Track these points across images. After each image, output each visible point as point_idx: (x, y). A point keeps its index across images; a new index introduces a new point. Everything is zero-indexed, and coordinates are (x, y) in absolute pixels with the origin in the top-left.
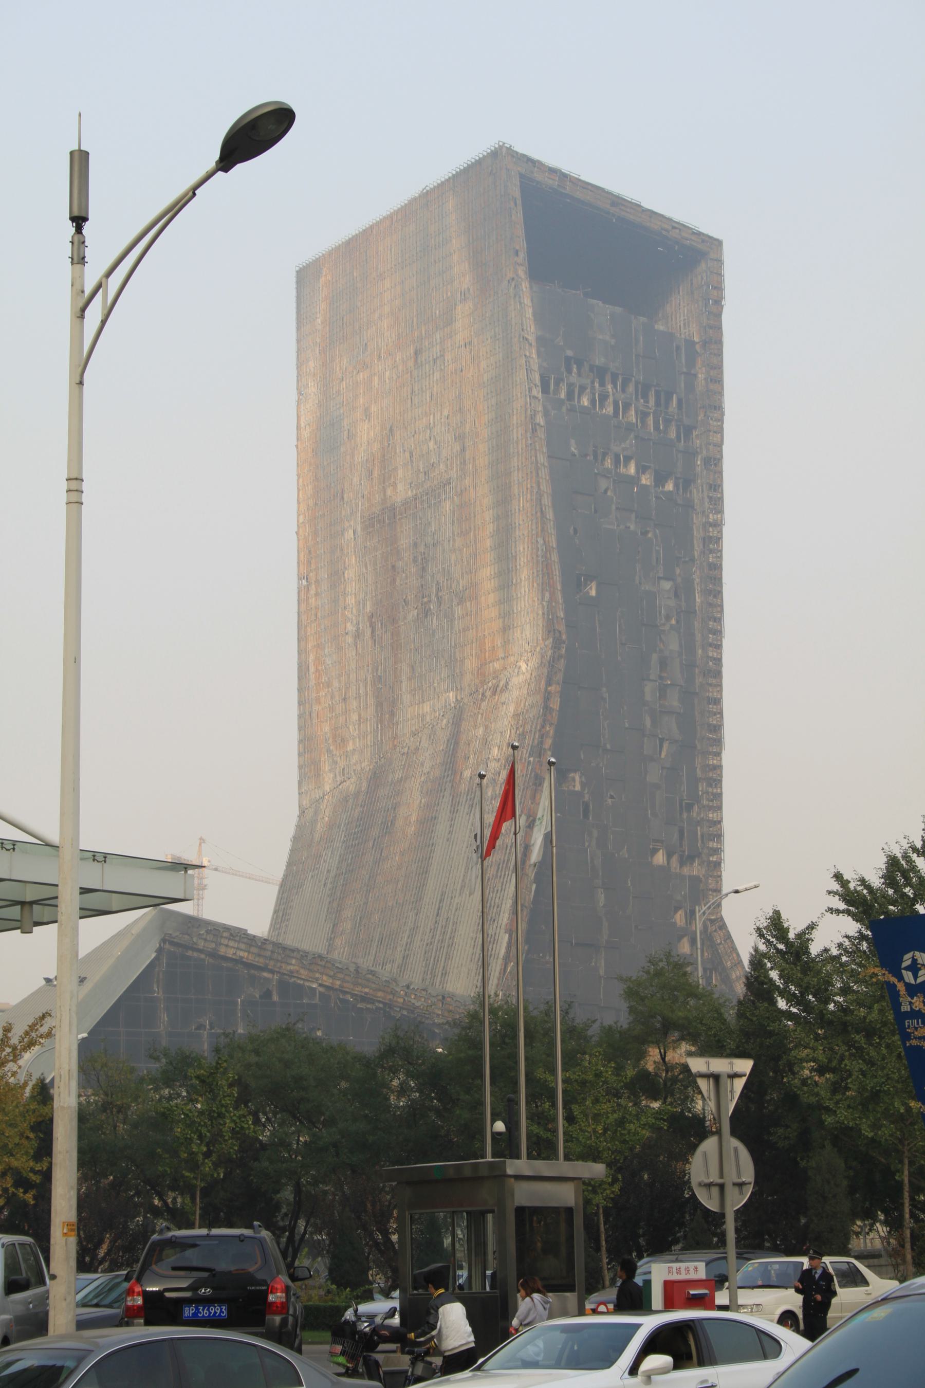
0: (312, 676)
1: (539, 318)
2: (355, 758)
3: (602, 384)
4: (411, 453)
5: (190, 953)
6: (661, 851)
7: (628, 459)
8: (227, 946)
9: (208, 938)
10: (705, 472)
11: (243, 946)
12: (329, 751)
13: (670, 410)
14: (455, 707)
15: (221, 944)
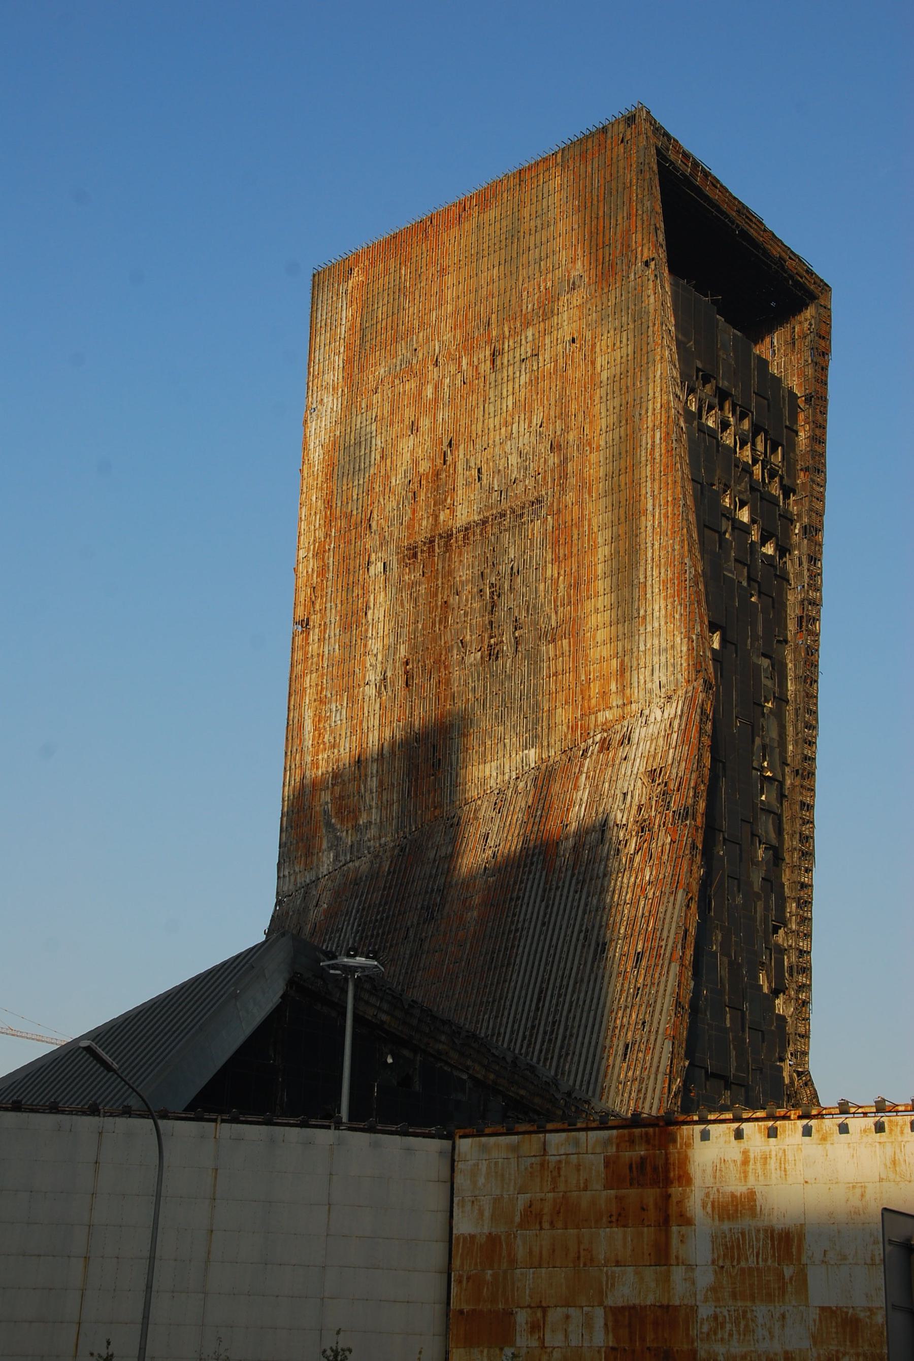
2: (373, 832)
4: (479, 471)
7: (743, 504)
11: (385, 1006)
12: (329, 825)
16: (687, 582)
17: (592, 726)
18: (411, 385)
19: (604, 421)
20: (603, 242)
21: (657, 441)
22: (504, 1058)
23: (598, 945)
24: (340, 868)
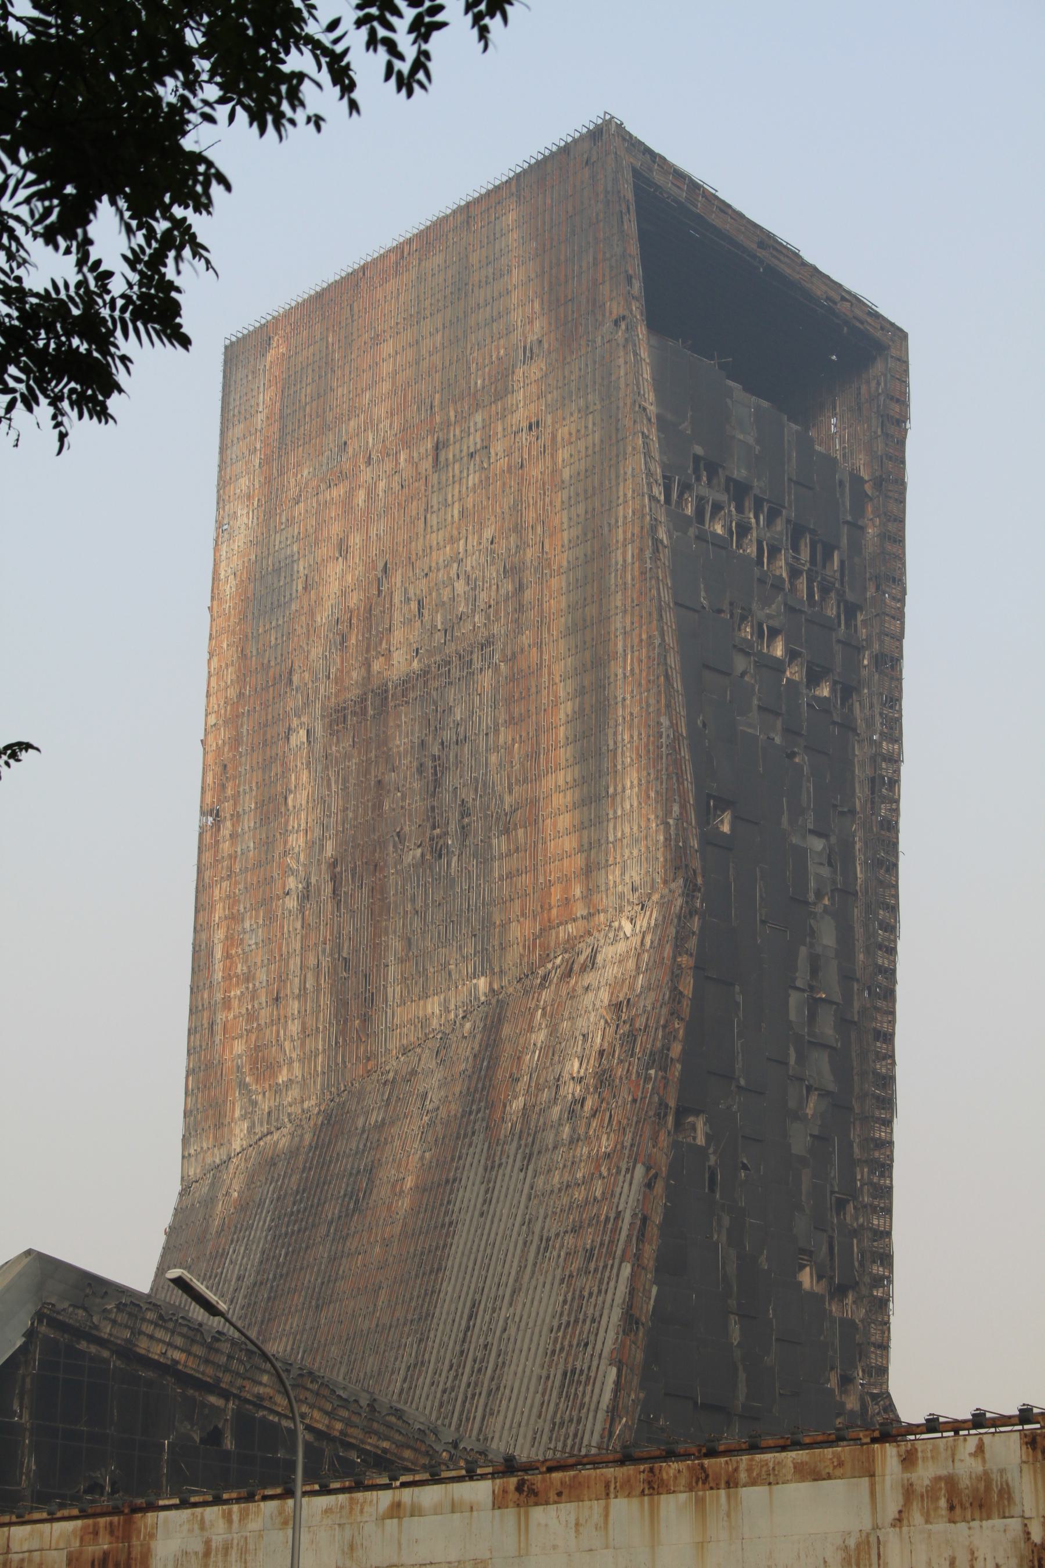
0: (218, 966)
1: (659, 385)
2: (294, 1093)
3: (740, 509)
4: (420, 604)
5: (83, 1345)
6: (808, 1269)
7: (774, 633)
8: (151, 1337)
9: (119, 1319)
10: (876, 677)
11: (179, 1341)
12: (243, 1085)
13: (828, 572)
14: (488, 1003)
15: (141, 1333)
16: (663, 749)
17: (552, 944)
18: (338, 492)
19: (565, 534)
20: (566, 296)
21: (629, 560)
22: (356, 1401)
23: (541, 1240)
24: (256, 1143)
